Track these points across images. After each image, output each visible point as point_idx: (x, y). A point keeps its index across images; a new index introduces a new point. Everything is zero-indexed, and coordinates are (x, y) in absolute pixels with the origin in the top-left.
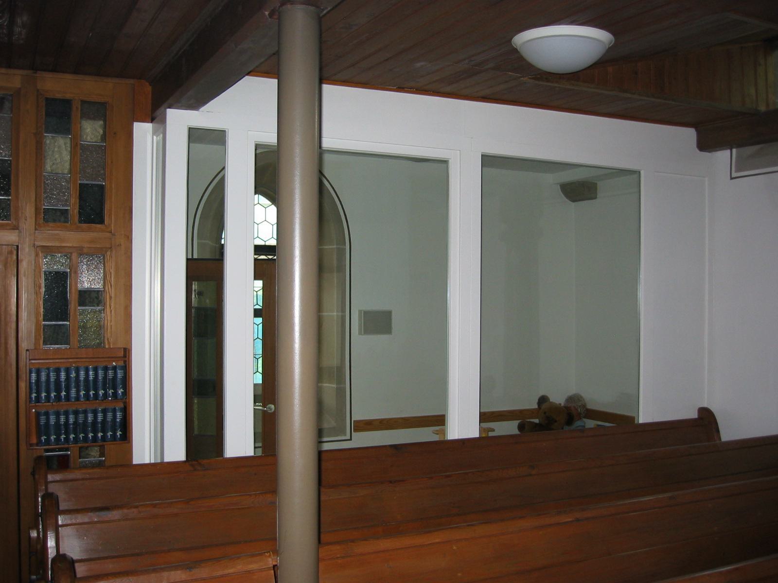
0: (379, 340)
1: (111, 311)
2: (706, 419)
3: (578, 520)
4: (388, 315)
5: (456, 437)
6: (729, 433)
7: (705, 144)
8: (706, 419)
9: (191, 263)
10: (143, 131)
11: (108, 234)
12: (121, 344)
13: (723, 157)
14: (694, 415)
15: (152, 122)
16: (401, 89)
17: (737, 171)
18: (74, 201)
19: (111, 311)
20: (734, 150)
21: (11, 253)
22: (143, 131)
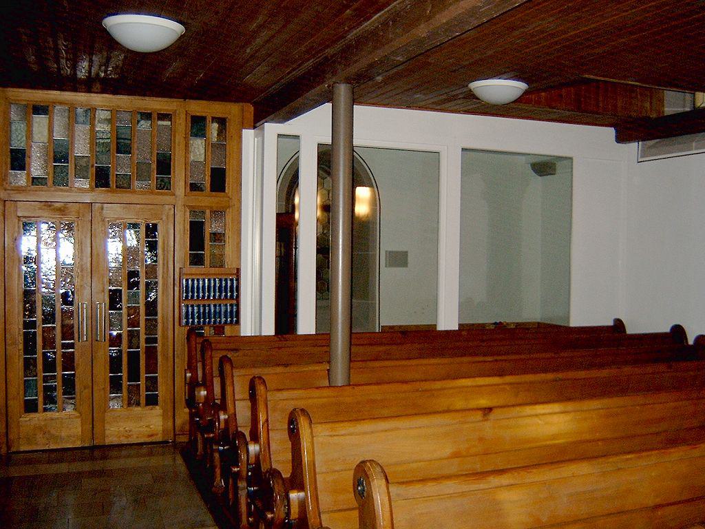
0: (399, 271)
1: (405, 392)
2: (619, 325)
3: (496, 361)
4: (405, 254)
5: (443, 329)
6: (630, 331)
7: (622, 138)
8: (619, 325)
9: (278, 215)
10: (248, 135)
11: (227, 199)
12: (235, 266)
13: (633, 147)
14: (611, 323)
15: (254, 128)
16: (408, 107)
17: (642, 157)
18: (208, 178)
19: (405, 392)
20: (640, 143)
21: (170, 209)
22: (248, 135)
